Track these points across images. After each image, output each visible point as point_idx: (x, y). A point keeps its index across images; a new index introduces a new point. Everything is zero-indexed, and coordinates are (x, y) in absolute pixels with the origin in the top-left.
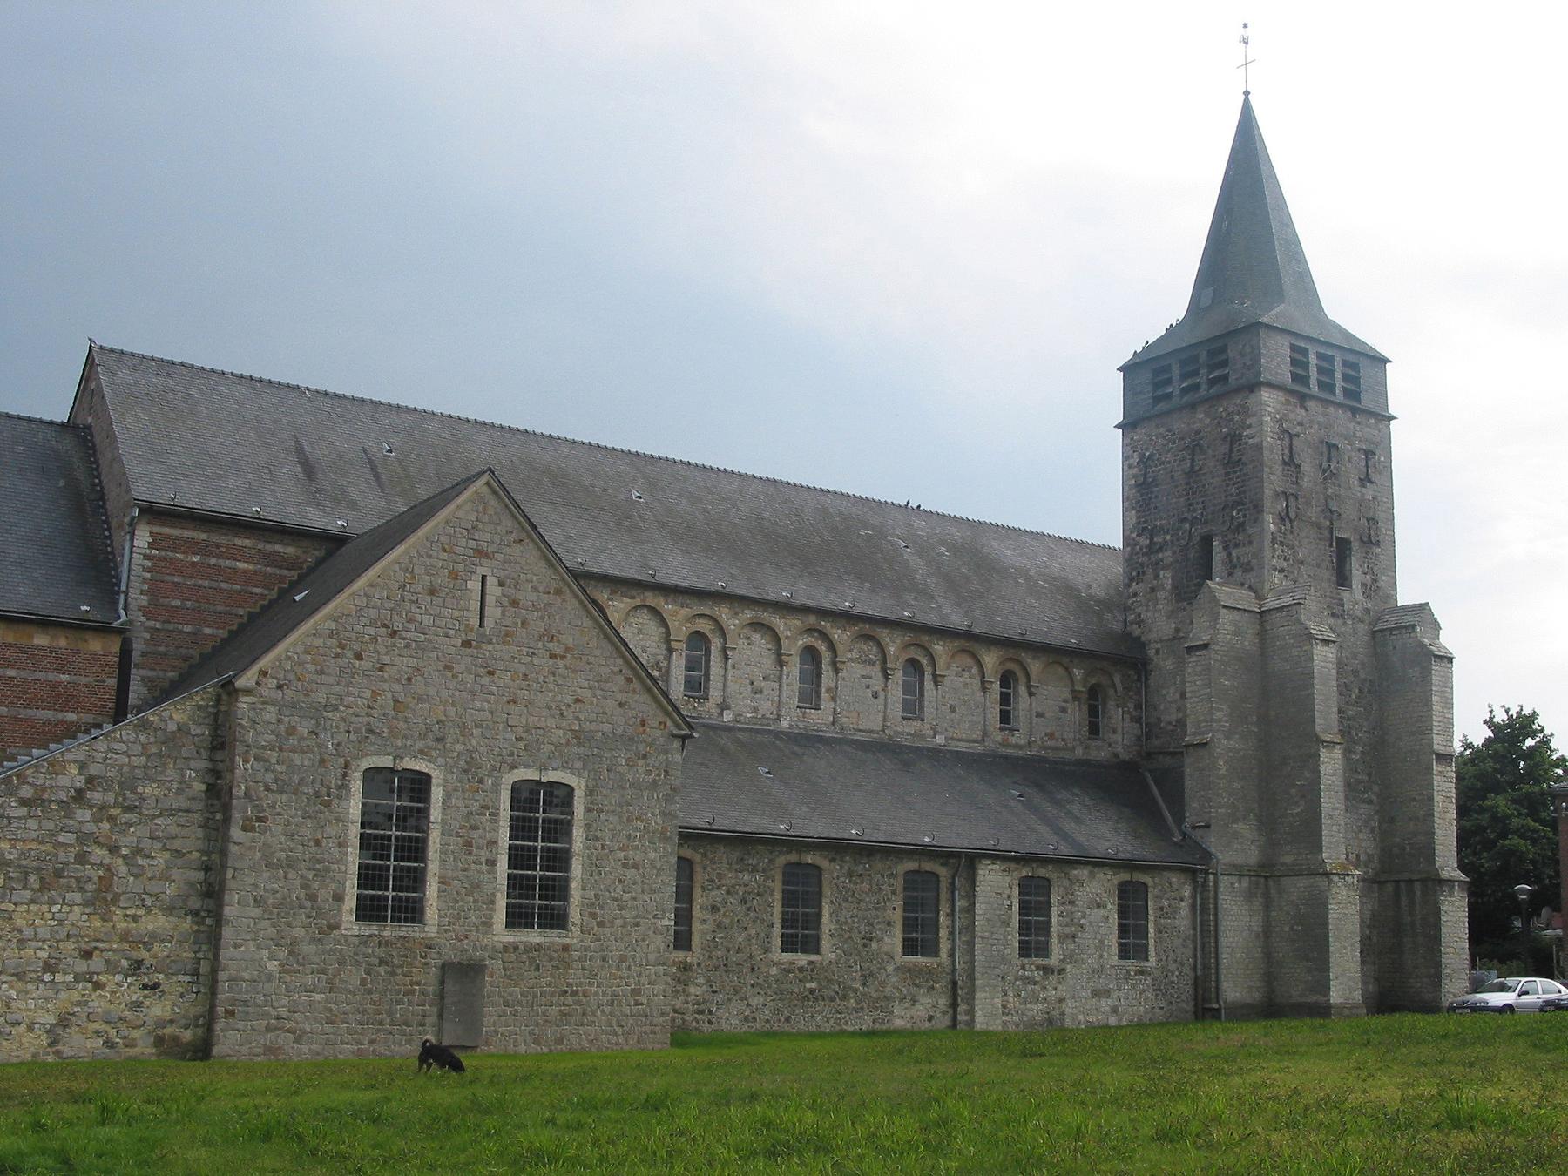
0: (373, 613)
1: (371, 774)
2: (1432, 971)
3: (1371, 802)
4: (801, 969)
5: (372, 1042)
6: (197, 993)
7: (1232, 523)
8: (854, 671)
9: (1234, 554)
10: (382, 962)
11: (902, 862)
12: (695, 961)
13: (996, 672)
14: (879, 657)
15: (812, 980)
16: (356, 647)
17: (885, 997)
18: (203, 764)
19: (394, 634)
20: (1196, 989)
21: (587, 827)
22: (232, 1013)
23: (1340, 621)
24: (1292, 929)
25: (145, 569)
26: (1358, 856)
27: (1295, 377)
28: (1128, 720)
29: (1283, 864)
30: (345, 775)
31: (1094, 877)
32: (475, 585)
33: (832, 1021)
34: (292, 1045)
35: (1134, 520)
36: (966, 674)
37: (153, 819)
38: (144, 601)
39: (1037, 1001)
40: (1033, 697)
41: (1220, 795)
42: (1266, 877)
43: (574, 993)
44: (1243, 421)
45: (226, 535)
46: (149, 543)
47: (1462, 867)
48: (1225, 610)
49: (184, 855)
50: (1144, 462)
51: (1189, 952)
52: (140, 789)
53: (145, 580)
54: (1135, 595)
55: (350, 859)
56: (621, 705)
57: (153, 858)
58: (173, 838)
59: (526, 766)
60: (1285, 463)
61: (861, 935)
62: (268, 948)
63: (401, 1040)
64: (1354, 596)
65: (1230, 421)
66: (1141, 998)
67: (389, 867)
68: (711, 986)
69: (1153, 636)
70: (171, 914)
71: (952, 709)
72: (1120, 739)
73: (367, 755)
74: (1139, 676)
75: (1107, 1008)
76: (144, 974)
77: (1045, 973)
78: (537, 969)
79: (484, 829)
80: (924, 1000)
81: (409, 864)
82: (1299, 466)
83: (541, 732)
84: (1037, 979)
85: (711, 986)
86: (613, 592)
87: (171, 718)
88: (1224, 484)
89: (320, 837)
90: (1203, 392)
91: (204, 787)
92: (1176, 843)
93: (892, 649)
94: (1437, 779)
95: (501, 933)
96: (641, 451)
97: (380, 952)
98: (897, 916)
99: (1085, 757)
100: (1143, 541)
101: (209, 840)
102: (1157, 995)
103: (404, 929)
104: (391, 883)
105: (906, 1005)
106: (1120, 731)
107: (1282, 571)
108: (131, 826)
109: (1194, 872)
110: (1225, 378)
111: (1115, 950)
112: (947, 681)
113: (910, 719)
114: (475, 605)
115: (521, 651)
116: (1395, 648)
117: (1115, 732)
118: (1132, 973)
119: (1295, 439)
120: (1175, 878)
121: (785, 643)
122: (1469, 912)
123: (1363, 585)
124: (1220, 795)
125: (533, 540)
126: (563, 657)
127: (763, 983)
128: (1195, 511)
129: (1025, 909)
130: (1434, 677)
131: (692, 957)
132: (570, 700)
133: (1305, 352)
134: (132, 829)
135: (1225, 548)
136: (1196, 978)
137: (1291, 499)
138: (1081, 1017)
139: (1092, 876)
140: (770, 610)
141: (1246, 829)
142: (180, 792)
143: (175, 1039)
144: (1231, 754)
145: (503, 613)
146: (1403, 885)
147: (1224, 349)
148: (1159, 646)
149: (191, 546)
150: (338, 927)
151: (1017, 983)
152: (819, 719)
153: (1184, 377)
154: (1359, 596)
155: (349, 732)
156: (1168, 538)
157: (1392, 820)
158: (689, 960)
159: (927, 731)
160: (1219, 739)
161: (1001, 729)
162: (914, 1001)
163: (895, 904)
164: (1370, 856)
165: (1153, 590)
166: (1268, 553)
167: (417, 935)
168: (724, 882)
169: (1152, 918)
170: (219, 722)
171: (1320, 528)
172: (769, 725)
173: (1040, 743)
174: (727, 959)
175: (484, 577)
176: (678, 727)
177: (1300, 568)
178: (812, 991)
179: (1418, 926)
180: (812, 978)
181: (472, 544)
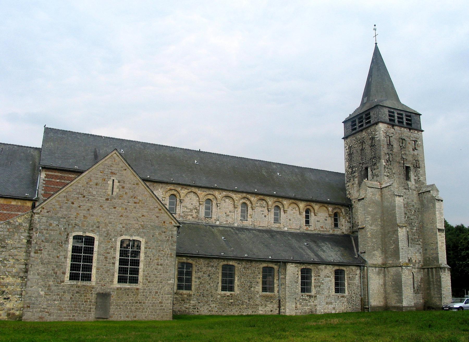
0: (78, 191)
1: (75, 238)
2: (439, 296)
3: (420, 244)
4: (228, 296)
5: (73, 316)
6: (21, 301)
7: (373, 163)
8: (258, 209)
9: (374, 172)
10: (77, 292)
11: (262, 264)
12: (193, 293)
13: (304, 209)
14: (267, 205)
15: (231, 299)
16: (72, 200)
17: (256, 304)
18: (26, 234)
19: (84, 197)
20: (361, 302)
21: (145, 253)
22: (29, 307)
23: (407, 191)
24: (392, 283)
25: (43, 184)
26: (416, 261)
27: (390, 120)
28: (347, 222)
29: (389, 264)
30: (67, 237)
31: (326, 268)
32: (110, 182)
33: (238, 312)
34: (47, 316)
35: (348, 165)
36: (294, 210)
37: (10, 250)
38: (43, 192)
39: (307, 306)
40: (316, 216)
41: (368, 243)
42: (384, 268)
43: (140, 303)
44: (375, 133)
45: (67, 174)
46: (45, 177)
47: (448, 263)
48: (369, 188)
49: (19, 260)
50: (350, 148)
51: (359, 291)
52: (7, 241)
53: (43, 187)
54: (348, 186)
55: (68, 262)
56: (157, 217)
57: (9, 261)
58: (16, 256)
59: (126, 235)
60: (388, 145)
61: (248, 286)
62: (41, 287)
63: (83, 316)
64: (412, 183)
65: (371, 134)
66: (343, 305)
67: (81, 264)
68: (198, 301)
69: (353, 198)
70: (14, 277)
71: (290, 220)
72: (344, 227)
73: (75, 232)
74: (350, 209)
75: (331, 308)
76: (5, 295)
77: (310, 297)
78: (128, 295)
79: (112, 253)
80: (269, 305)
81: (122, 266)
82: (392, 146)
83: (131, 225)
84: (307, 299)
85: (198, 301)
86: (182, 188)
87: (17, 221)
88: (370, 152)
89: (59, 255)
90: (364, 126)
91: (26, 241)
92: (356, 258)
93: (270, 203)
94: (438, 237)
95: (116, 284)
96: (331, 171)
97: (77, 289)
98: (260, 281)
99: (333, 233)
100: (350, 170)
101: (27, 256)
102: (348, 304)
103: (85, 283)
104: (81, 269)
105: (263, 307)
106: (344, 225)
107: (387, 176)
108: (3, 252)
109: (360, 266)
110: (370, 122)
111: (334, 290)
112: (288, 212)
113: (276, 223)
114: (110, 188)
115: (125, 201)
116: (425, 198)
117: (343, 226)
118: (340, 297)
119: (391, 138)
120: (354, 268)
121: (236, 202)
122: (451, 277)
123: (415, 180)
124: (368, 243)
125: (129, 169)
126: (138, 203)
127: (215, 300)
128: (363, 160)
129: (303, 278)
130: (436, 206)
131: (192, 292)
132: (141, 216)
133: (393, 113)
134: (3, 253)
135: (371, 171)
136: (361, 298)
137: (390, 155)
138: (322, 311)
139: (326, 268)
140: (231, 192)
141: (378, 253)
142: (19, 242)
143: (14, 314)
144: (372, 231)
145: (119, 190)
146: (430, 269)
147: (369, 114)
148: (355, 200)
149: (57, 177)
150: (63, 282)
151: (300, 300)
152: (248, 223)
153: (360, 122)
154: (414, 183)
155: (69, 225)
156: (356, 169)
157: (426, 250)
158: (191, 293)
159: (282, 226)
160: (368, 226)
161: (306, 226)
162: (266, 306)
163: (259, 277)
164: (420, 262)
165: (353, 184)
166: (383, 171)
167: (89, 284)
168: (202, 270)
169: (346, 280)
170: (32, 222)
171: (400, 163)
172: (231, 225)
173: (318, 229)
174: (203, 293)
175: (113, 180)
176: (176, 223)
177: (394, 175)
178: (232, 303)
179: (435, 282)
180: (231, 299)
181: (110, 171)
